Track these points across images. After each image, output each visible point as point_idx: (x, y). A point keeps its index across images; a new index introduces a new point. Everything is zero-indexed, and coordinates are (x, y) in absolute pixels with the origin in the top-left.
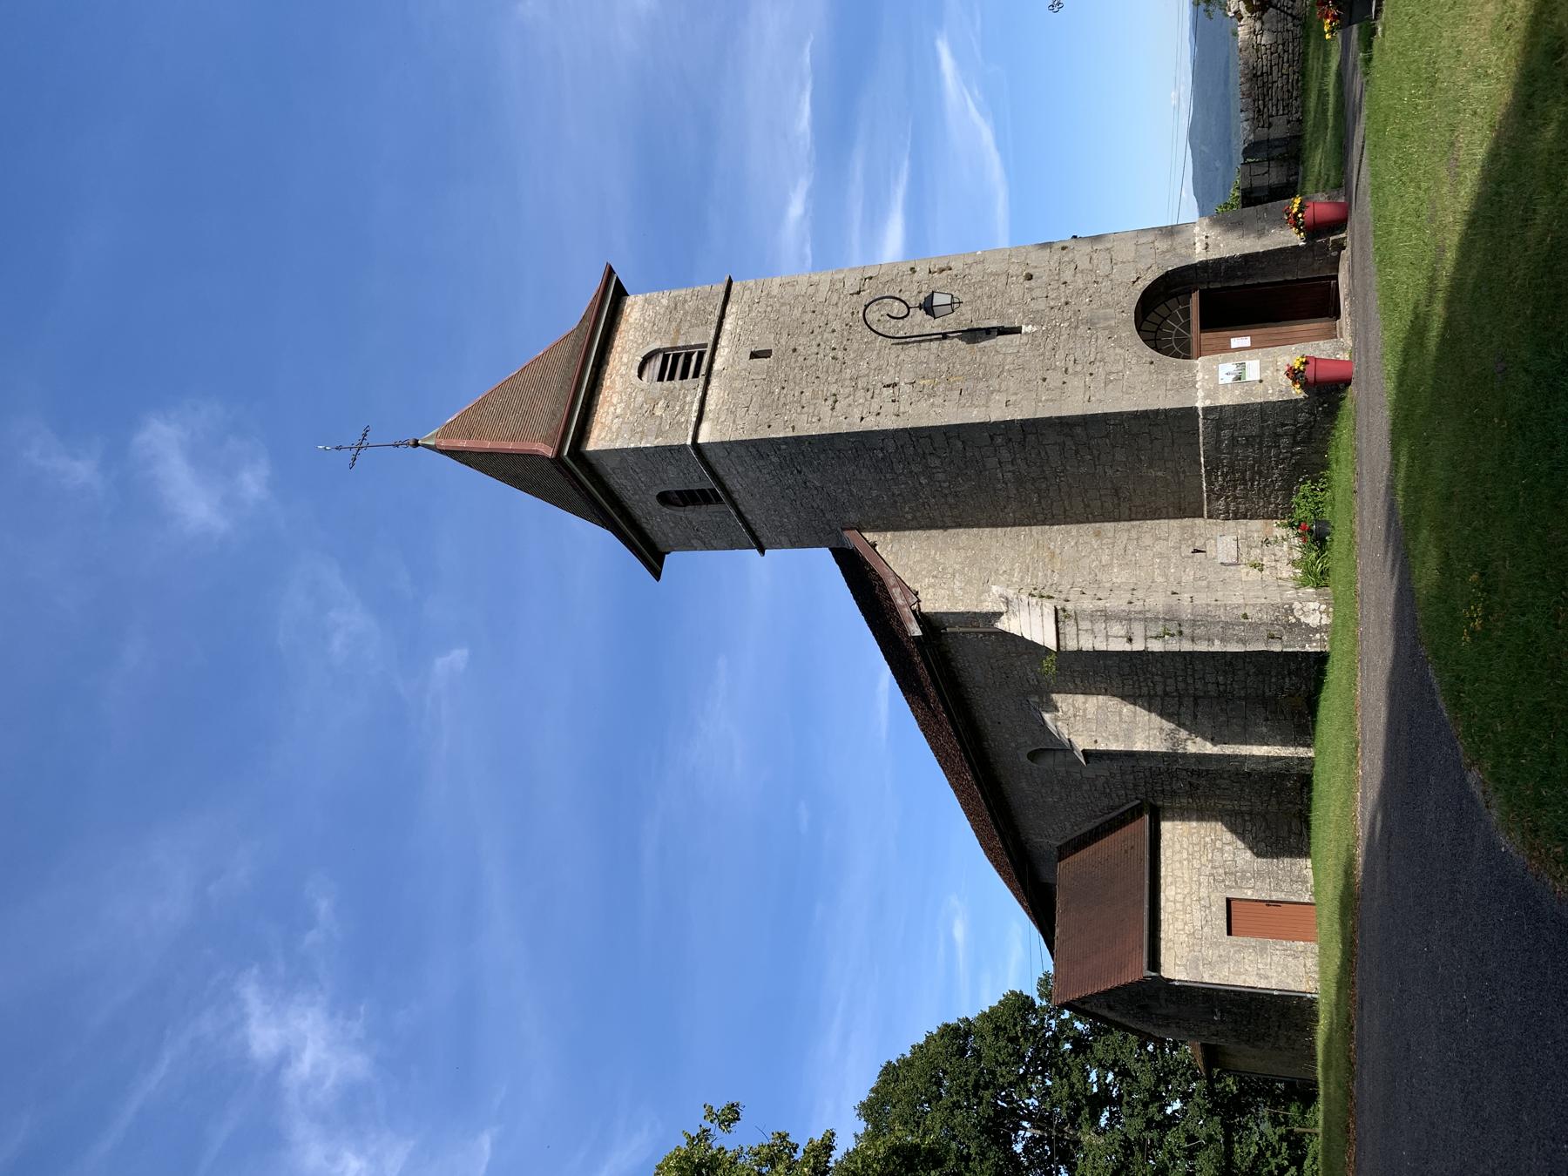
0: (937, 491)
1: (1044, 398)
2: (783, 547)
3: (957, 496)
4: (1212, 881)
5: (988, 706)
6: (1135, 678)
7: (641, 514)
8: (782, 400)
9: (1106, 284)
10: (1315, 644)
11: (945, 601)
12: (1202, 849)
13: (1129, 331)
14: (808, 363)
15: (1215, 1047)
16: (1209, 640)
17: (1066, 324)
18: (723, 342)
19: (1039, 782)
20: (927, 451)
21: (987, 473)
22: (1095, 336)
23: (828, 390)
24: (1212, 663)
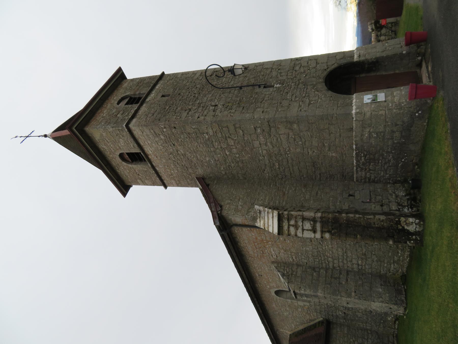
0: (234, 159)
1: (280, 110)
2: (174, 186)
3: (243, 162)
5: (256, 267)
6: (320, 258)
7: (115, 165)
8: (168, 111)
9: (313, 70)
10: (412, 242)
11: (233, 211)
13: (322, 86)
14: (183, 98)
16: (354, 236)
17: (294, 84)
18: (154, 92)
19: (280, 305)
20: (227, 136)
21: (255, 150)
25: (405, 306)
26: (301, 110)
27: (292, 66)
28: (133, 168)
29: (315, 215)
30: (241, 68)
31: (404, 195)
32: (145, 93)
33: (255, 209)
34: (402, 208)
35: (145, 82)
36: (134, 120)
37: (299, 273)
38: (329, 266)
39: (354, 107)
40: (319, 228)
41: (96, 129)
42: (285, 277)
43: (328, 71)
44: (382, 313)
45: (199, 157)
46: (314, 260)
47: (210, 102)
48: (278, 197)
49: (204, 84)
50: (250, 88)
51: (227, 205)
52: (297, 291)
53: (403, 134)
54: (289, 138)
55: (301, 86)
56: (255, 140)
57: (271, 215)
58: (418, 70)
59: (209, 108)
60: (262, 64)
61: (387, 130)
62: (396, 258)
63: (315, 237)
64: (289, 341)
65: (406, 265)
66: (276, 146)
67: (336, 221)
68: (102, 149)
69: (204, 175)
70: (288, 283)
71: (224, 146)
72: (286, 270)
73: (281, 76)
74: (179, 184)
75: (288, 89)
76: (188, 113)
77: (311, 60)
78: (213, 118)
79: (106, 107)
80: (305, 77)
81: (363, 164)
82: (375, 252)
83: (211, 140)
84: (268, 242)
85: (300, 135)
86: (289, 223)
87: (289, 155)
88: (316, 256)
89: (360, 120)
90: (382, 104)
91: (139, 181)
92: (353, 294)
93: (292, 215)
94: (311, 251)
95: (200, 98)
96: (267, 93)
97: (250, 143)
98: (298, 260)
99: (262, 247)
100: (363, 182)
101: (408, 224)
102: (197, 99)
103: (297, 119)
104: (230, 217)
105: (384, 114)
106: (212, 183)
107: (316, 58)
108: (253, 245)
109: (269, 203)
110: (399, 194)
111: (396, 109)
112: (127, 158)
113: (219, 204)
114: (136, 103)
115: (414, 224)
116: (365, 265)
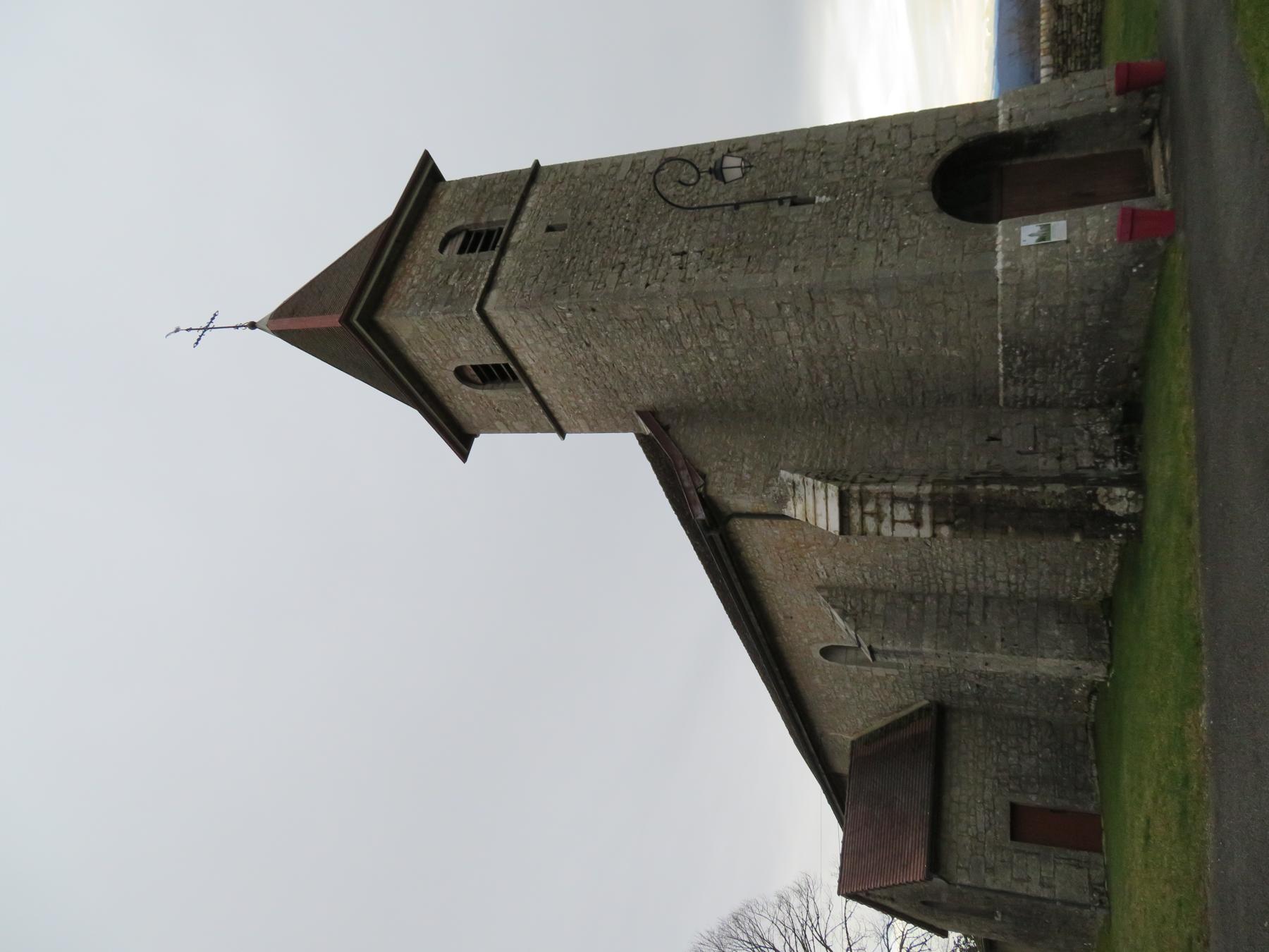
1: (833, 264)
2: (582, 432)
3: (747, 375)
4: (996, 784)
5: (780, 599)
7: (442, 392)
9: (904, 156)
10: (1120, 535)
11: (732, 484)
12: (988, 751)
13: (927, 201)
14: (601, 234)
15: (995, 942)
17: (861, 194)
18: (524, 217)
20: (714, 323)
21: (777, 349)
22: (889, 205)
23: (616, 259)
24: (1004, 559)
25: (1109, 662)
26: (881, 262)
27: (853, 145)
28: (486, 397)
29: (918, 490)
30: (739, 165)
31: (1107, 432)
32: (506, 220)
33: (781, 479)
34: (1103, 463)
35: (494, 188)
36: (494, 294)
37: (880, 605)
38: (946, 590)
39: (1000, 256)
40: (928, 516)
41: (404, 318)
42: (847, 618)
43: (938, 158)
44: (1060, 679)
45: (646, 369)
46: (912, 578)
47: (668, 243)
48: (831, 450)
49: (644, 196)
50: (761, 206)
51: (716, 471)
52: (877, 646)
53: (1107, 309)
54: (856, 323)
55: (876, 199)
56: (777, 330)
57: (821, 494)
58: (1144, 147)
59: (669, 260)
60: (780, 138)
61: (1072, 303)
62: (1090, 565)
63: (919, 535)
64: (852, 754)
65: (1111, 579)
66: (825, 339)
67: (962, 500)
68: (415, 360)
69: (657, 406)
70: (856, 631)
71: (705, 343)
72: (850, 603)
73: (828, 172)
74: (595, 427)
75: (848, 208)
76: (620, 275)
77: (896, 126)
78: (681, 286)
79: (412, 261)
80: (885, 175)
81: (1020, 370)
82: (1044, 555)
83: (675, 331)
84: (808, 546)
85: (881, 316)
86: (862, 509)
87: (854, 358)
88: (918, 570)
89: (1013, 285)
90: (1060, 248)
91: (497, 423)
92: (998, 644)
93: (869, 492)
94: (905, 561)
95: (641, 233)
96: (801, 220)
97: (766, 335)
98: (876, 579)
99: (796, 558)
100: (1018, 406)
101: (1112, 501)
102: (635, 237)
103: (875, 285)
104: (726, 499)
105: (1064, 270)
106: (675, 422)
107: (908, 122)
108: (776, 553)
109: (811, 464)
110: (1098, 431)
111: (1091, 261)
112: (472, 375)
113: (698, 471)
114: (484, 249)
115: (1125, 499)
116: (1023, 583)
